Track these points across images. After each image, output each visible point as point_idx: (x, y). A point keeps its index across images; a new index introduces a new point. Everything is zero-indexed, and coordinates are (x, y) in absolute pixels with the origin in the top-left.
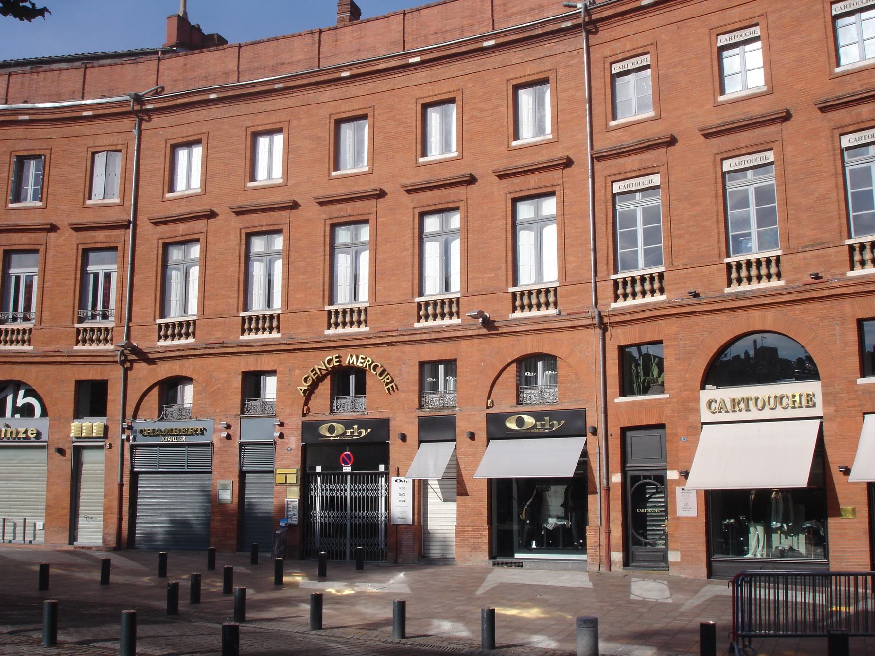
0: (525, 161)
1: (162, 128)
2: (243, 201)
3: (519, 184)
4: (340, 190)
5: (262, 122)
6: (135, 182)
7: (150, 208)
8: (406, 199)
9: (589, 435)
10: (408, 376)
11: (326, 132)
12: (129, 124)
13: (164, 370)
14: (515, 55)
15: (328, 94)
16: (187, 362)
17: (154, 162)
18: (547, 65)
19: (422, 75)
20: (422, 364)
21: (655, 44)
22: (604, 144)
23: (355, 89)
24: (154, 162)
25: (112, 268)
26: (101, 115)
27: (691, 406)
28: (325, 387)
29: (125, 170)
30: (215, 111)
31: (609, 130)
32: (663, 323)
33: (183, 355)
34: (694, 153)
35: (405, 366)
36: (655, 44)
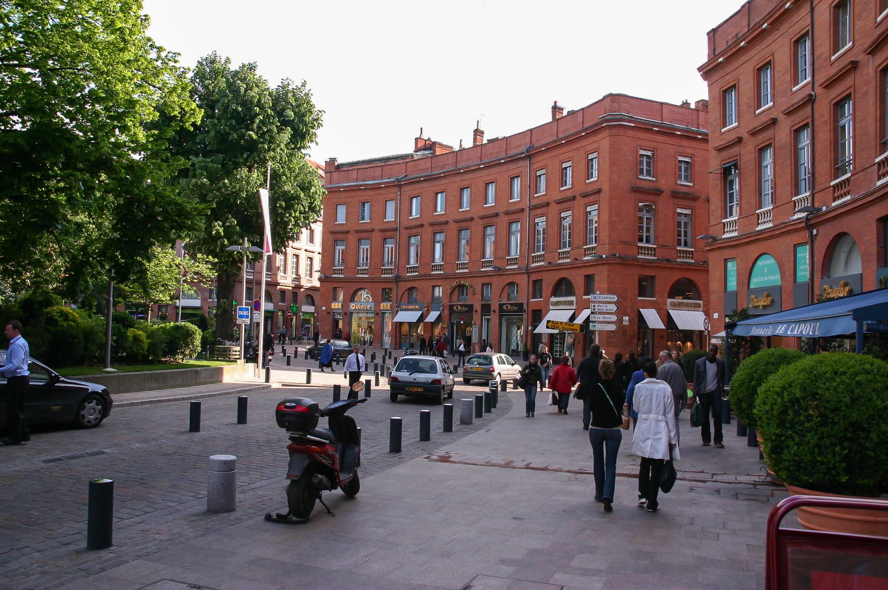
0: (513, 208)
1: (408, 190)
2: (432, 220)
3: (437, 228)
4: (461, 217)
5: (439, 189)
6: (398, 211)
7: (405, 224)
8: (479, 220)
9: (495, 306)
10: (478, 288)
11: (457, 193)
12: (395, 190)
13: (409, 285)
14: (511, 166)
15: (458, 178)
16: (416, 282)
17: (406, 204)
18: (519, 170)
19: (485, 172)
20: (483, 285)
21: (598, 148)
22: (533, 203)
23: (467, 177)
24: (406, 204)
25: (368, 247)
26: (389, 186)
27: (547, 303)
28: (456, 292)
29: (396, 208)
30: (424, 185)
31: (534, 198)
32: (564, 271)
33: (413, 279)
34: (554, 208)
35: (478, 283)
36: (598, 148)
